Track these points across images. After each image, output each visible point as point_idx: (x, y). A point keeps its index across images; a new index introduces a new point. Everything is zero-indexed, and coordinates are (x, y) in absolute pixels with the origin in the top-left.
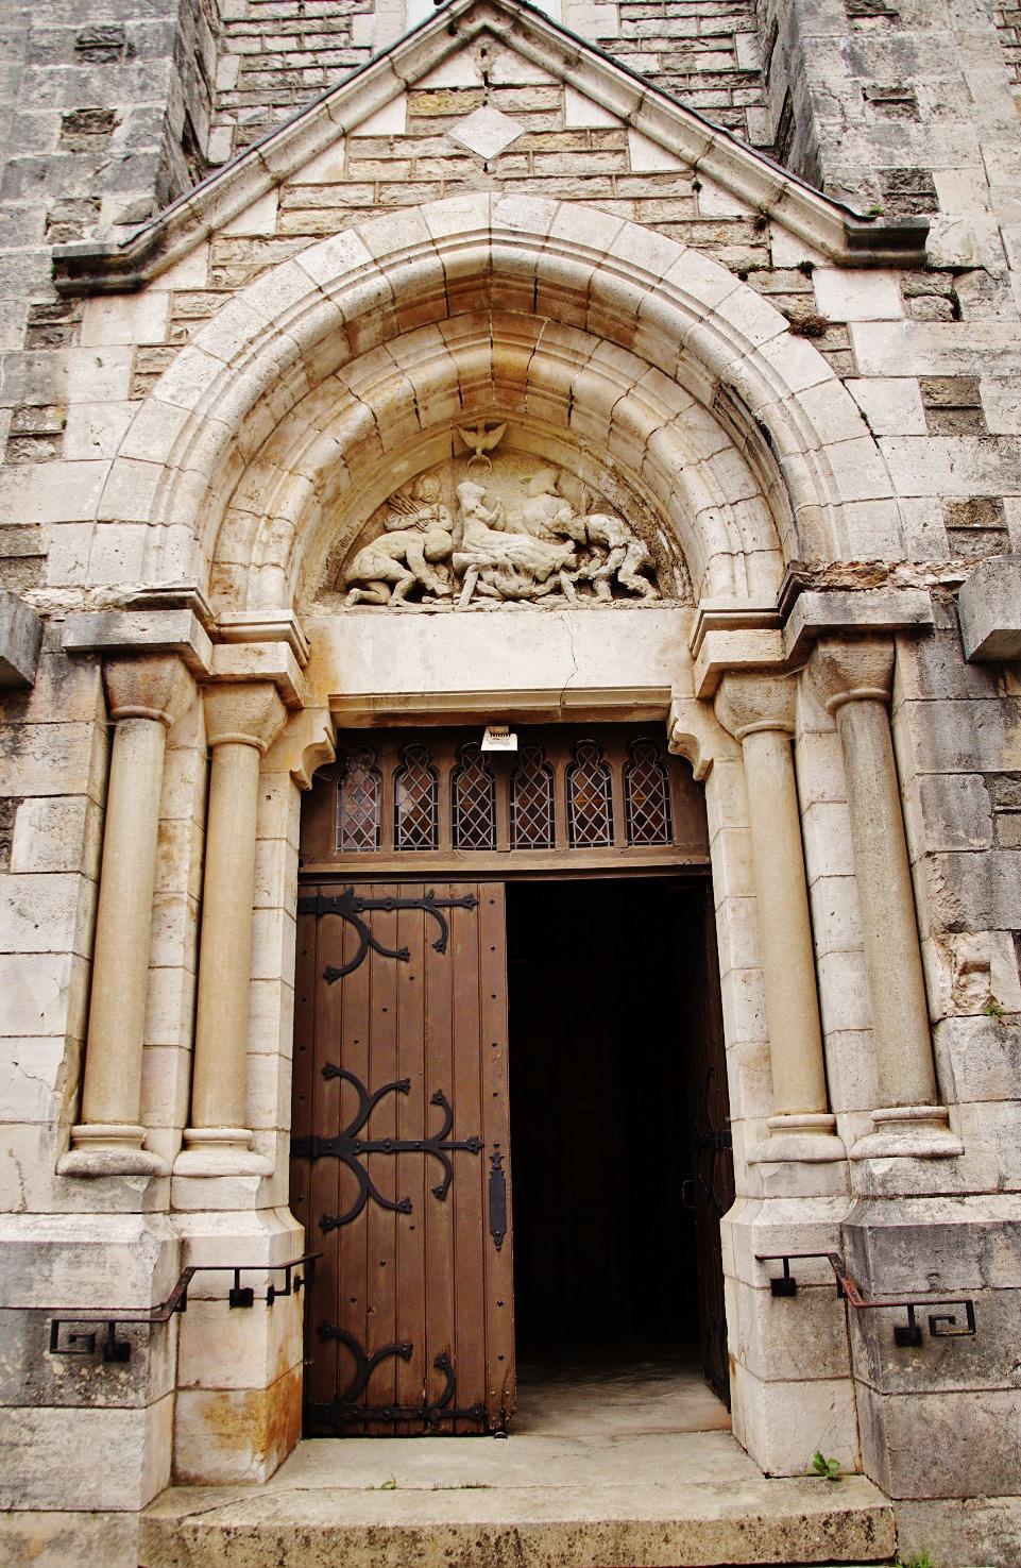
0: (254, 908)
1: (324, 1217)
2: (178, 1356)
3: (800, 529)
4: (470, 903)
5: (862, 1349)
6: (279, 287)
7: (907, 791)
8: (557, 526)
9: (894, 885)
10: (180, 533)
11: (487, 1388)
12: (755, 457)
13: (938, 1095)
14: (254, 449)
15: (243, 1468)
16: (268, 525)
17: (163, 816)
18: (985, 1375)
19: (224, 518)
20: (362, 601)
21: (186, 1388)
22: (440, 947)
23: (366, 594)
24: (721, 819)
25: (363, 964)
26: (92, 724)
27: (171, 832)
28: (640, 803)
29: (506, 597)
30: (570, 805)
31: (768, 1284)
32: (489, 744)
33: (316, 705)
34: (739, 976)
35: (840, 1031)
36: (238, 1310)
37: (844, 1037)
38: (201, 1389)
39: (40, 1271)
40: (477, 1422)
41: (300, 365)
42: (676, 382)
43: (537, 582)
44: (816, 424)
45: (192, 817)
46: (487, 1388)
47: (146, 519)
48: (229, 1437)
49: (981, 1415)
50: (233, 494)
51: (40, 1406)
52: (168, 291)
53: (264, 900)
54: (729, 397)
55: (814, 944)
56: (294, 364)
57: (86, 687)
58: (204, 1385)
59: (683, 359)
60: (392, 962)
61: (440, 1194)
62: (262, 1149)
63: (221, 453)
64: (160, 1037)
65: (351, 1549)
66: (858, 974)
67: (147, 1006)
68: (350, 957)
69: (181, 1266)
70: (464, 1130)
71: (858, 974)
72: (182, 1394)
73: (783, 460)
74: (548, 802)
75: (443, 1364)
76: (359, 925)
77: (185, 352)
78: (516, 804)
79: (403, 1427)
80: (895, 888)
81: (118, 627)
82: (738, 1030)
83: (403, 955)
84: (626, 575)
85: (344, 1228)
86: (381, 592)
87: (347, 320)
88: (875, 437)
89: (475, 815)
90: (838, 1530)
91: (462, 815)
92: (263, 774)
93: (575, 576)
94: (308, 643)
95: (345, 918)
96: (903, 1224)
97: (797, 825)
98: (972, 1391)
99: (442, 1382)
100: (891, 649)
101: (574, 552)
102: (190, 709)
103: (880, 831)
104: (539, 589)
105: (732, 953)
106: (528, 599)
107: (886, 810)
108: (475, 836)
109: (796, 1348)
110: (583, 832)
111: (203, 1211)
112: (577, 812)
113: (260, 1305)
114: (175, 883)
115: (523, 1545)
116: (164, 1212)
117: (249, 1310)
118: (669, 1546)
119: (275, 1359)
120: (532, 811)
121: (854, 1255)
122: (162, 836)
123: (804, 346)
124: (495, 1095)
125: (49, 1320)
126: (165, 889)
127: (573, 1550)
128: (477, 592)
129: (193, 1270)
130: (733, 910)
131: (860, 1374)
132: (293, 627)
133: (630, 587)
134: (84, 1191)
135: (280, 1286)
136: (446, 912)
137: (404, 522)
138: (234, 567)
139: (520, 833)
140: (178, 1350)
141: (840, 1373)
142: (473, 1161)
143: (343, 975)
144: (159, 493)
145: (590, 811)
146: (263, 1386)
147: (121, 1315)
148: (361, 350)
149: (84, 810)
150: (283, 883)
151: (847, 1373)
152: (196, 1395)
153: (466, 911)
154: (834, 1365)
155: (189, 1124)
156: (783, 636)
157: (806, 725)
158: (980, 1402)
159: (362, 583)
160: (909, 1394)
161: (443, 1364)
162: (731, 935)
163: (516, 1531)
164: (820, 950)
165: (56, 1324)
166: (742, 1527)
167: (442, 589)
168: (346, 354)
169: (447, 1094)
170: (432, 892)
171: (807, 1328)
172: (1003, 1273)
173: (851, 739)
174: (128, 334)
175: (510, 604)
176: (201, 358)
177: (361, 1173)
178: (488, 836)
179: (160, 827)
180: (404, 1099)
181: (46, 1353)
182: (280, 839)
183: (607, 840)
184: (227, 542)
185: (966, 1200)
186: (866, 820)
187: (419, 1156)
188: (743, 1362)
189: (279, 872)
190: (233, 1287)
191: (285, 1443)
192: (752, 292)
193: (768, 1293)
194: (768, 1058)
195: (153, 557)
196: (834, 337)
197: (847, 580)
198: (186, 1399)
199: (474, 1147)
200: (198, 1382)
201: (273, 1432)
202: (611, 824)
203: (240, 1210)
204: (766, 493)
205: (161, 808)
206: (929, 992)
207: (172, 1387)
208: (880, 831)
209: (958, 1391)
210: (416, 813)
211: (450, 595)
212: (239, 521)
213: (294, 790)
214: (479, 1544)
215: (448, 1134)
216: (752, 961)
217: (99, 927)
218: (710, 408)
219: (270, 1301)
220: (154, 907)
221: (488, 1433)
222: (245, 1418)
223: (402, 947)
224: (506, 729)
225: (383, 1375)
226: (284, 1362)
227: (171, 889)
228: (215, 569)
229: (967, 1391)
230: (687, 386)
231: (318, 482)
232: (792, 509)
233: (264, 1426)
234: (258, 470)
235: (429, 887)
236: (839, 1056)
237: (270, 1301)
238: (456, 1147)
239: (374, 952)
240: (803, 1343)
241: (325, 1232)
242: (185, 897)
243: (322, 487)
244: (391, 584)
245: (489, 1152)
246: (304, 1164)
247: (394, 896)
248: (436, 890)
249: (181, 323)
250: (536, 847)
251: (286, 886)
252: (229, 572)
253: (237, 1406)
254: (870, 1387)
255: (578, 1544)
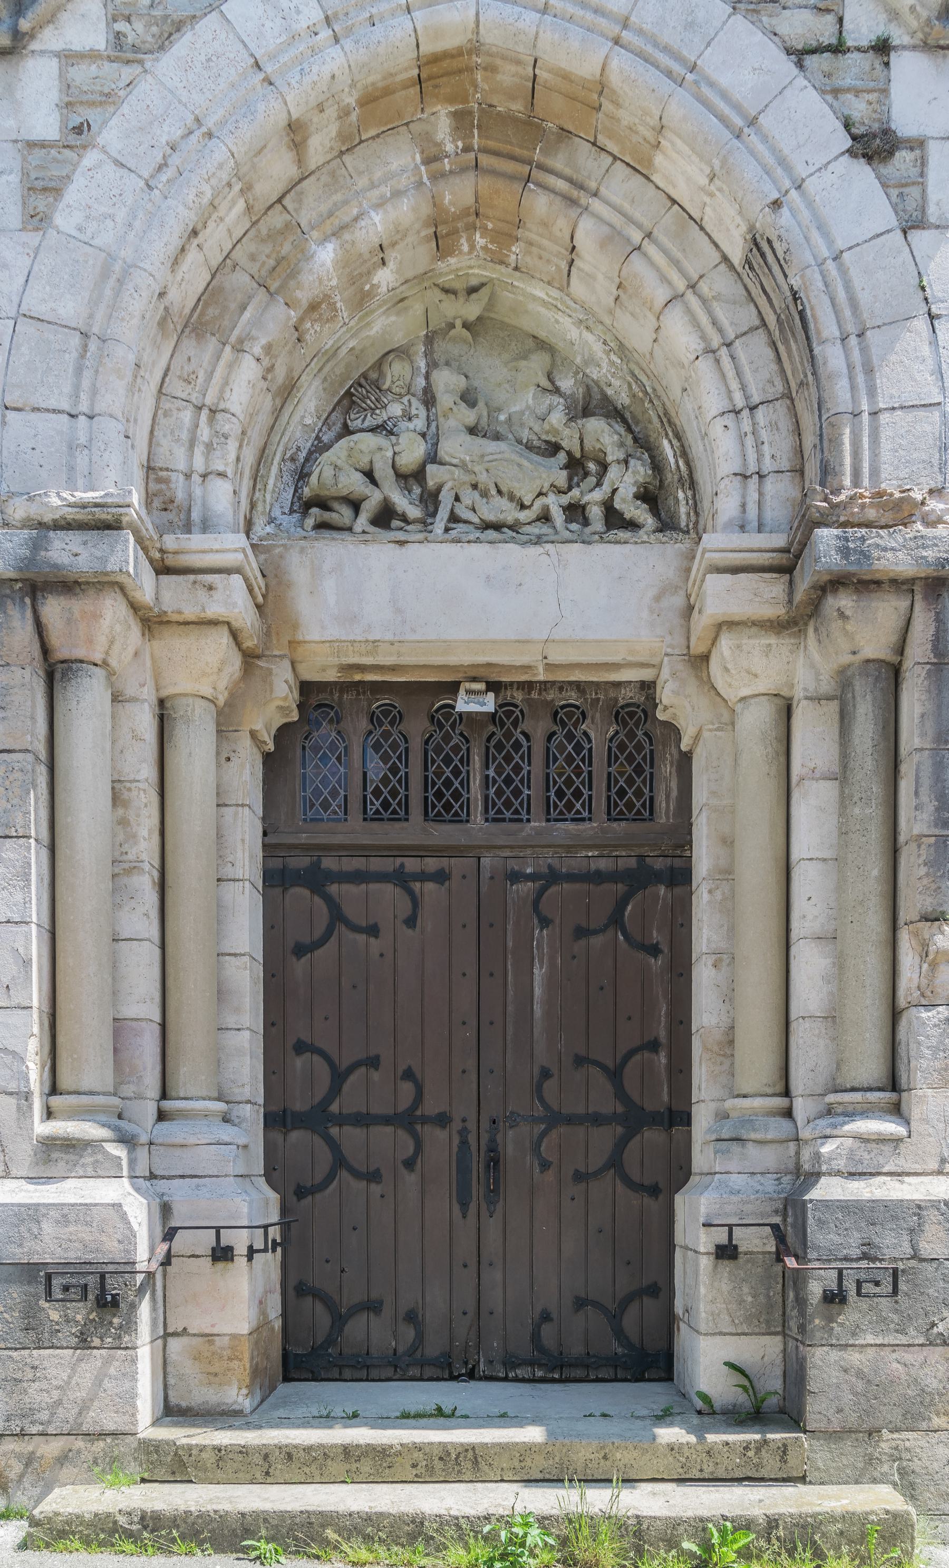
0: (219, 880)
1: (299, 1186)
2: (165, 1306)
3: (826, 444)
4: (441, 877)
5: (793, 1308)
6: (203, 58)
7: (903, 768)
8: (547, 433)
9: (875, 869)
10: (111, 429)
11: (451, 1340)
12: (786, 342)
13: (893, 1083)
14: (187, 311)
15: (230, 1401)
16: (211, 420)
17: (116, 777)
18: (902, 1332)
19: (157, 408)
20: (322, 526)
21: (175, 1334)
22: (411, 922)
23: (327, 516)
24: (705, 794)
25: (332, 939)
26: (28, 669)
27: (126, 795)
28: (622, 774)
29: (487, 526)
30: (548, 774)
31: (712, 1250)
32: (463, 705)
33: (276, 653)
34: (710, 960)
35: (803, 1018)
36: (220, 1265)
37: (807, 1024)
38: (189, 1335)
39: (29, 1230)
40: (443, 1368)
41: (237, 187)
42: (702, 228)
43: (523, 507)
44: (864, 298)
45: (147, 780)
46: (451, 1340)
47: (65, 406)
48: (216, 1375)
49: (895, 1365)
50: (165, 375)
51: (39, 1348)
52: (57, 55)
53: (229, 872)
54: (763, 255)
55: (788, 930)
56: (229, 185)
57: (16, 623)
58: (191, 1331)
59: (711, 195)
60: (362, 938)
61: (409, 1164)
62: (237, 1121)
63: (147, 316)
64: (131, 1010)
65: (329, 1462)
66: (829, 961)
67: (114, 979)
68: (318, 932)
69: (164, 1227)
70: (431, 1107)
71: (829, 961)
72: (170, 1340)
73: (817, 350)
74: (525, 772)
75: (411, 1317)
76: (328, 899)
77: (91, 158)
78: (491, 773)
79: (374, 1373)
80: (875, 872)
81: (47, 550)
82: (705, 1015)
83: (373, 931)
84: (624, 500)
85: (318, 1196)
86: (343, 514)
87: (294, 117)
88: (932, 317)
89: (448, 783)
90: (756, 1453)
91: (434, 784)
92: (222, 732)
93: (565, 500)
94: (264, 576)
95: (313, 892)
96: (842, 1198)
97: (785, 802)
98: (889, 1345)
99: (409, 1334)
100: (908, 603)
101: (566, 467)
102: (136, 654)
103: (868, 811)
104: (524, 516)
105: (705, 937)
106: (510, 528)
107: (877, 789)
108: (448, 807)
109: (733, 1306)
110: (561, 805)
111: (182, 1177)
112: (555, 782)
113: (241, 1262)
114: (134, 851)
115: (480, 1459)
116: (144, 1178)
117: (230, 1264)
118: (608, 1463)
119: (256, 1309)
120: (508, 781)
121: (794, 1226)
122: (117, 799)
123: (862, 172)
124: (464, 1072)
125: (42, 1274)
126: (125, 858)
127: (523, 1464)
128: (454, 518)
129: (175, 1230)
130: (710, 892)
131: (790, 1330)
132: (246, 556)
133: (627, 516)
134: (66, 1157)
135: (259, 1245)
136: (417, 886)
137: (370, 422)
138: (174, 476)
139: (494, 804)
140: (165, 1301)
141: (773, 1329)
142: (441, 1135)
143: (311, 951)
144: (79, 371)
145: (569, 782)
146: (246, 1332)
147: (111, 1268)
148: (313, 167)
149: (29, 767)
150: (247, 854)
151: (779, 1329)
152: (184, 1340)
153: (437, 886)
154: (768, 1322)
155: (164, 1096)
156: (791, 582)
157: (805, 689)
158: (894, 1356)
159: (323, 504)
160: (831, 1345)
161: (411, 1317)
162: (705, 918)
163: (473, 1449)
164: (794, 935)
165: (49, 1277)
166: (672, 1449)
167: (414, 512)
168: (293, 172)
169: (417, 1070)
170: (402, 865)
171: (746, 1289)
172: (932, 1245)
173: (850, 708)
174: (11, 123)
175: (491, 534)
176: (110, 167)
177: (333, 1145)
178: (461, 807)
179: (113, 788)
180: (375, 1076)
181: (43, 1303)
182: (243, 805)
183: (585, 814)
184: (164, 442)
185: (906, 1179)
186: (855, 799)
187: (389, 1129)
188: (686, 1319)
189: (243, 840)
190: (214, 1244)
191: (267, 1383)
192: (811, 89)
193: (712, 1258)
194: (731, 1042)
195: (82, 461)
196: (903, 159)
197: (871, 514)
198: (175, 1345)
199: (443, 1120)
200: (185, 1329)
201: (256, 1372)
202: (590, 797)
203: (217, 1176)
204: (794, 395)
205: (113, 768)
206: (897, 982)
207: (162, 1333)
208: (868, 811)
209: (876, 1345)
210: (385, 780)
211: (423, 522)
212: (175, 412)
213: (255, 750)
214: (441, 1459)
215: (417, 1108)
216: (723, 945)
217: (58, 897)
218: (740, 269)
219: (250, 1258)
220: (114, 876)
221: (453, 1378)
222: (230, 1359)
223: (371, 922)
224: (481, 686)
225: (356, 1328)
226: (263, 1313)
227: (130, 857)
228: (152, 476)
229: (884, 1345)
230: (715, 236)
231: (266, 362)
232: (820, 416)
233: (248, 1366)
234: (193, 342)
235: (399, 861)
236: (801, 1041)
237: (250, 1258)
238: (425, 1120)
239: (343, 928)
240: (741, 1302)
241: (299, 1200)
242: (147, 867)
243: (270, 369)
244: (356, 505)
245: (456, 1125)
246: (278, 1137)
247: (363, 868)
248: (407, 864)
249: (80, 109)
250: (511, 820)
251: (251, 857)
252: (167, 481)
253: (222, 1349)
254: (797, 1340)
255: (529, 1460)
